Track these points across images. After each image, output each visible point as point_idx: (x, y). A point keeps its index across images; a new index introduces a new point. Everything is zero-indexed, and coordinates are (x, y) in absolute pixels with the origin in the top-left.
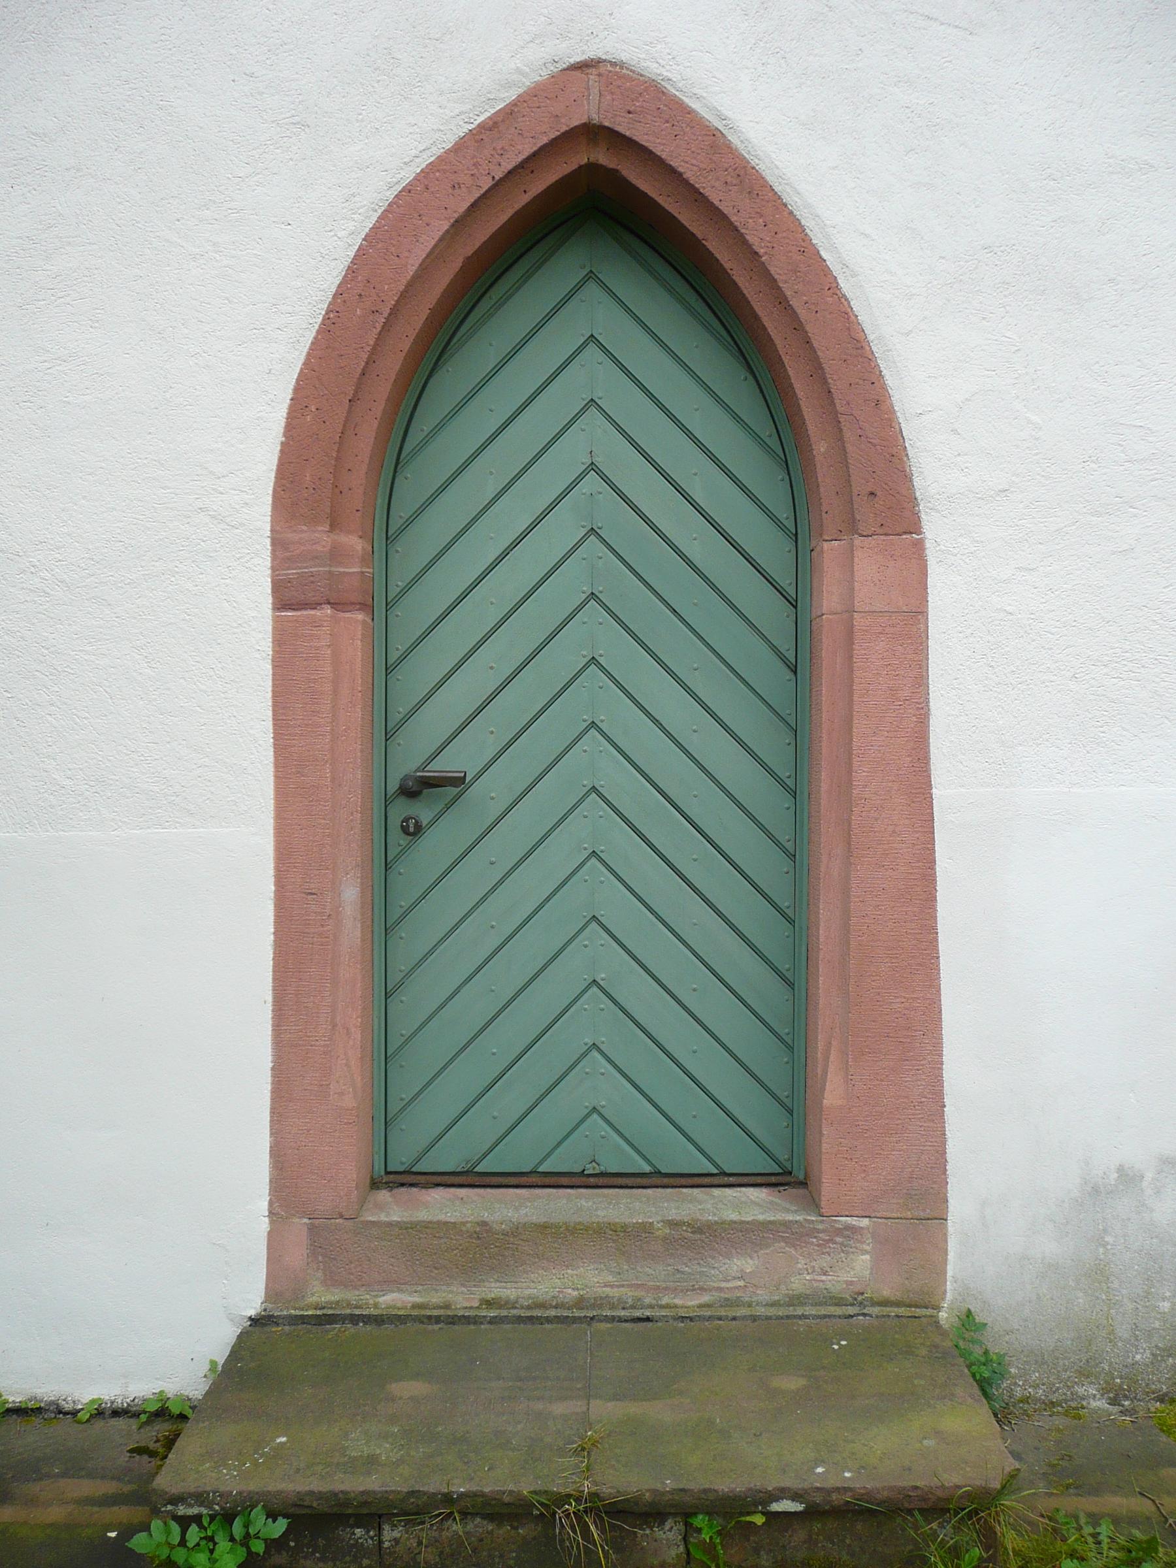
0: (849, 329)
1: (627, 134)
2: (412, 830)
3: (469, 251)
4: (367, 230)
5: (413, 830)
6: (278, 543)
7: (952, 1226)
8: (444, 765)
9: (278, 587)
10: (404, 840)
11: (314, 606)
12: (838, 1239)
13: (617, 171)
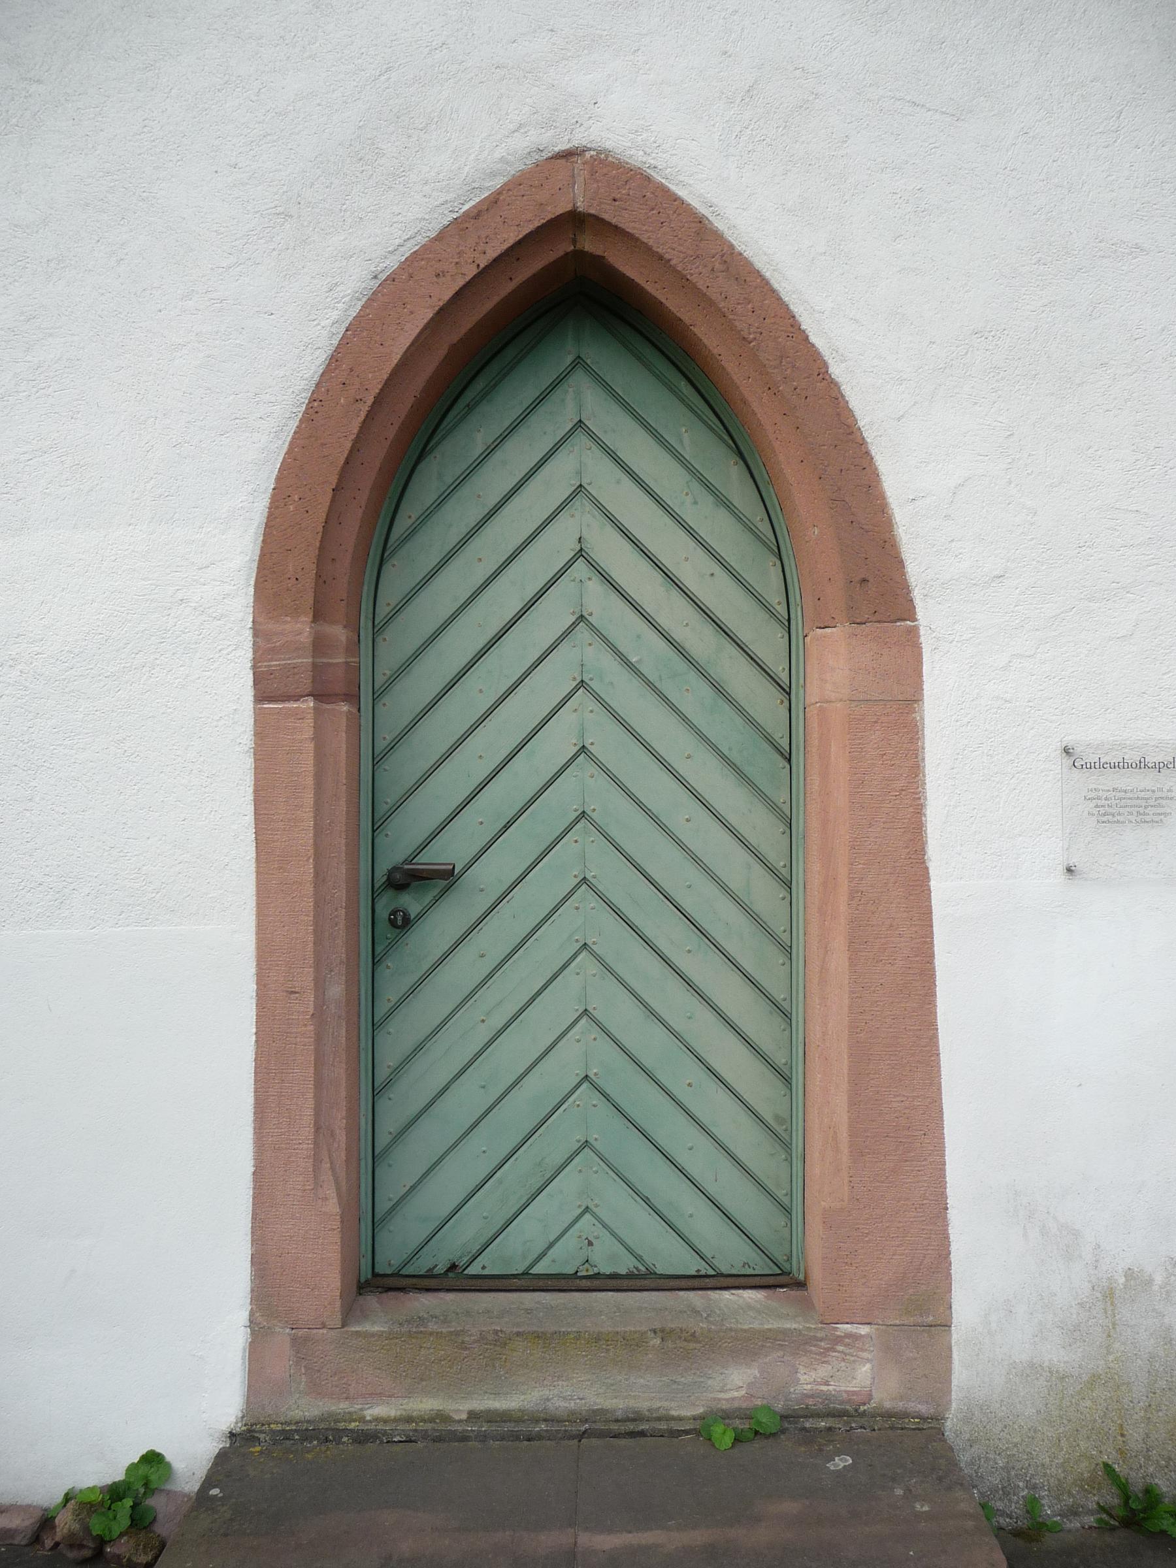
0: (838, 414)
1: (614, 221)
2: (400, 923)
3: (455, 338)
4: (350, 319)
5: (402, 923)
6: (256, 632)
7: (957, 1334)
8: (438, 855)
9: (259, 679)
10: (391, 933)
11: (297, 698)
12: (840, 1348)
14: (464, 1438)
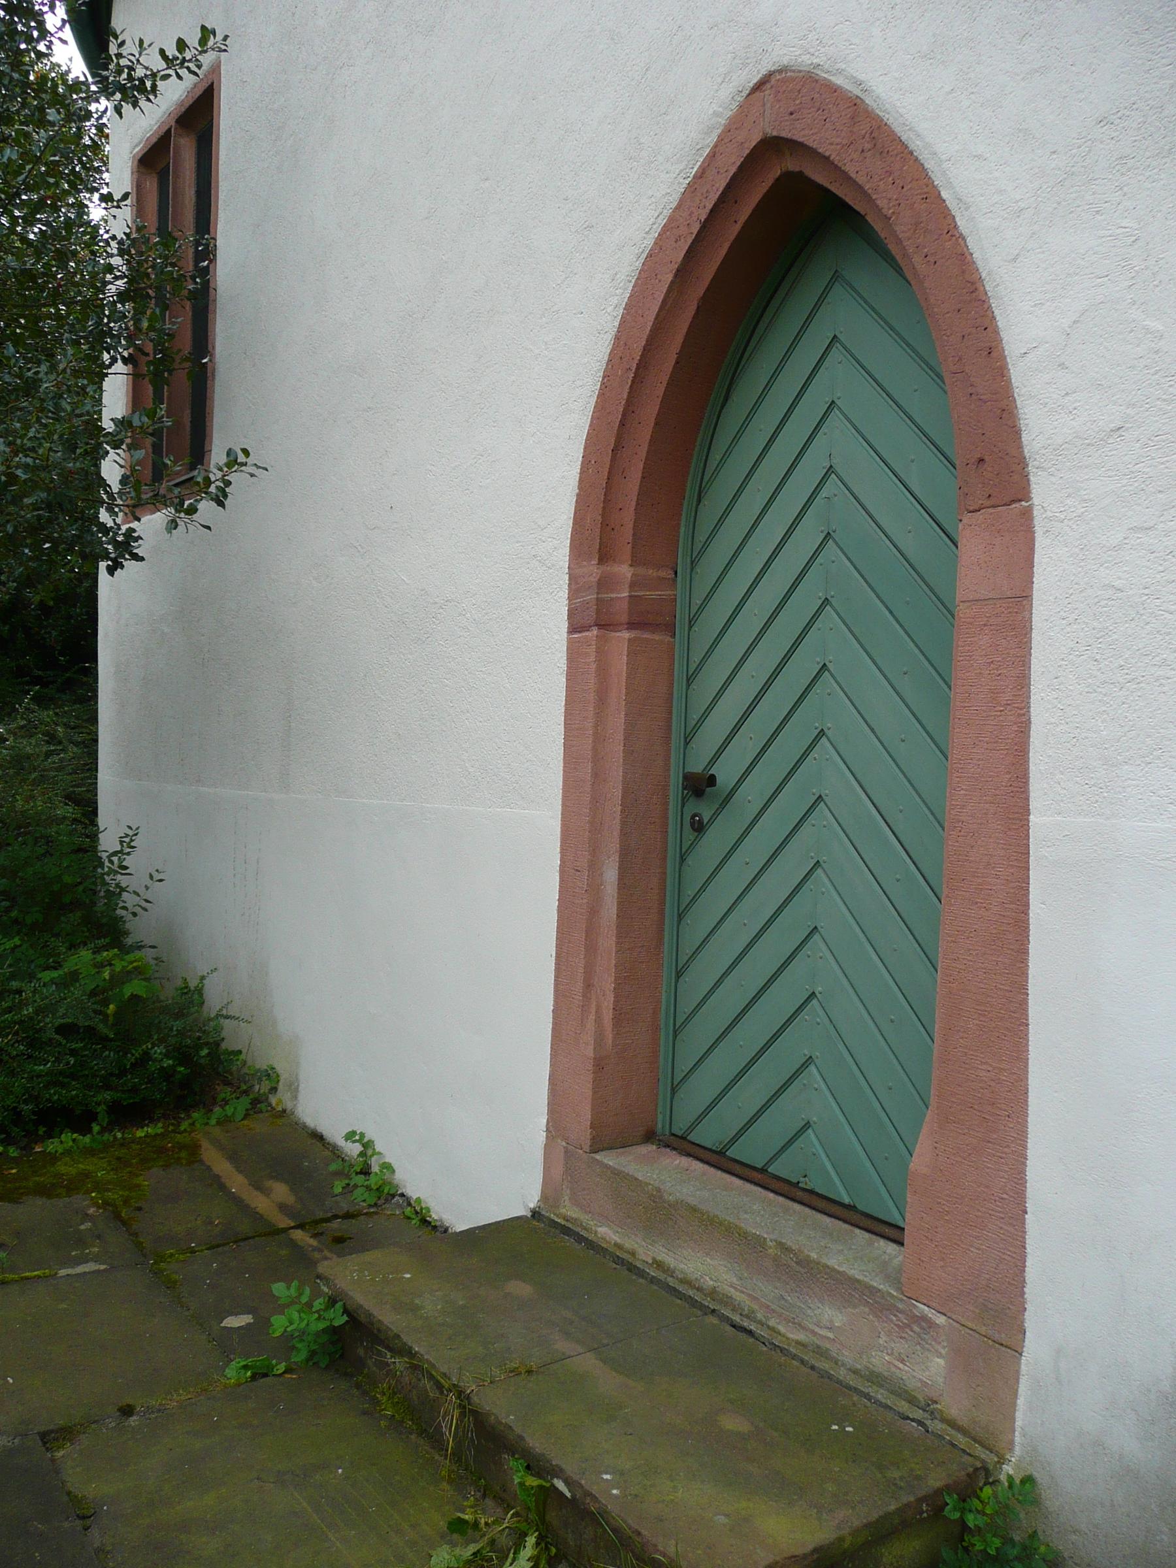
3: (701, 291)
5: (699, 827)
13: (801, 172)
14: (641, 1273)
